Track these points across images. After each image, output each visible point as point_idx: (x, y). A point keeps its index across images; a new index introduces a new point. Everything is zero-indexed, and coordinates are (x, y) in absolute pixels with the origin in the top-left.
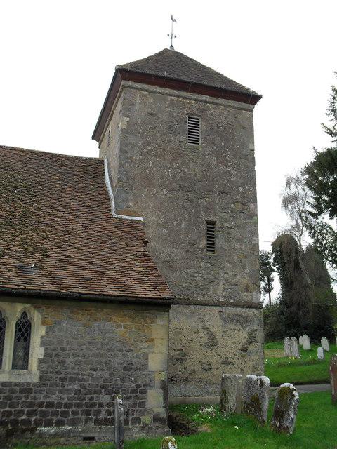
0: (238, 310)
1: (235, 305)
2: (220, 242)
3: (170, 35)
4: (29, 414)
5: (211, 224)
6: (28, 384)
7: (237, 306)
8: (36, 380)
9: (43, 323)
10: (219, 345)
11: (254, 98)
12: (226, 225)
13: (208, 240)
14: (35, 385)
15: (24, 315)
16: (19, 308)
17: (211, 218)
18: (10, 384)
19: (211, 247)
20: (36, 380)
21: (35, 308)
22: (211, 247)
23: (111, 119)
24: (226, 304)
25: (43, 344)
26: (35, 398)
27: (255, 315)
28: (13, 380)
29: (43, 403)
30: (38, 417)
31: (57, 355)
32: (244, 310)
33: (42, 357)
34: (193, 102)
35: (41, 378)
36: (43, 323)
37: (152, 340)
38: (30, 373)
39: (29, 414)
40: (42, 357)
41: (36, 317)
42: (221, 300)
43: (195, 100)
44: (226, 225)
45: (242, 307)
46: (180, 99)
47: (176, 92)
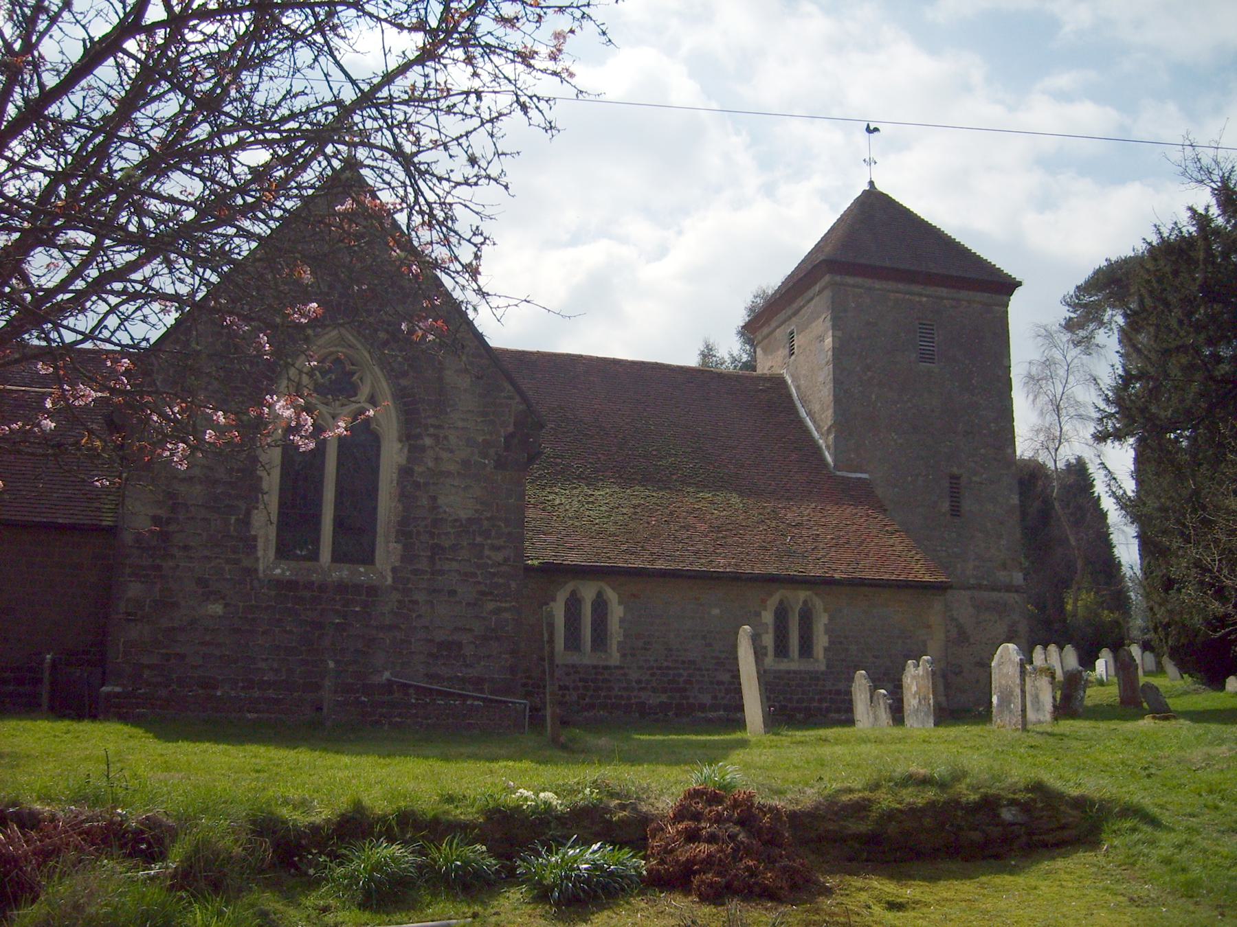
0: (995, 595)
1: (994, 588)
2: (968, 505)
3: (873, 164)
4: (820, 701)
5: (955, 478)
6: (817, 672)
7: (993, 590)
8: (823, 668)
9: (825, 610)
10: (972, 640)
11: (1008, 286)
12: (974, 479)
13: (952, 501)
14: (822, 673)
15: (600, 594)
16: (802, 594)
17: (955, 470)
18: (800, 672)
19: (955, 511)
20: (823, 668)
21: (816, 594)
22: (955, 511)
23: (795, 313)
24: (979, 587)
25: (827, 631)
26: (824, 686)
27: (1017, 602)
28: (802, 668)
29: (831, 691)
30: (828, 704)
31: (841, 643)
32: (1002, 594)
33: (827, 645)
34: (924, 299)
35: (828, 666)
36: (825, 610)
37: (929, 627)
38: (817, 661)
39: (820, 701)
40: (827, 645)
41: (818, 603)
42: (972, 581)
43: (926, 296)
44: (974, 479)
45: (999, 591)
46: (907, 297)
47: (901, 286)
